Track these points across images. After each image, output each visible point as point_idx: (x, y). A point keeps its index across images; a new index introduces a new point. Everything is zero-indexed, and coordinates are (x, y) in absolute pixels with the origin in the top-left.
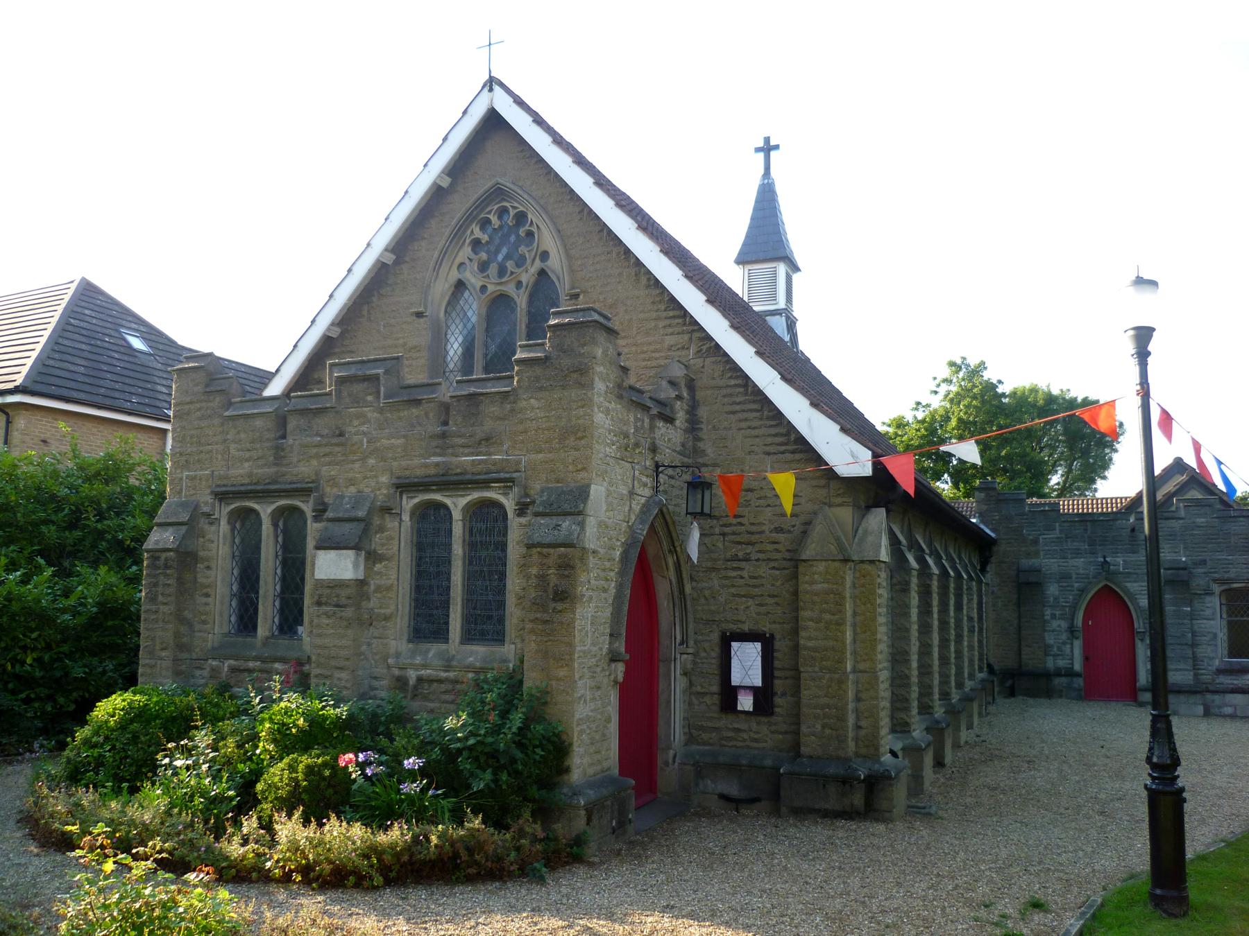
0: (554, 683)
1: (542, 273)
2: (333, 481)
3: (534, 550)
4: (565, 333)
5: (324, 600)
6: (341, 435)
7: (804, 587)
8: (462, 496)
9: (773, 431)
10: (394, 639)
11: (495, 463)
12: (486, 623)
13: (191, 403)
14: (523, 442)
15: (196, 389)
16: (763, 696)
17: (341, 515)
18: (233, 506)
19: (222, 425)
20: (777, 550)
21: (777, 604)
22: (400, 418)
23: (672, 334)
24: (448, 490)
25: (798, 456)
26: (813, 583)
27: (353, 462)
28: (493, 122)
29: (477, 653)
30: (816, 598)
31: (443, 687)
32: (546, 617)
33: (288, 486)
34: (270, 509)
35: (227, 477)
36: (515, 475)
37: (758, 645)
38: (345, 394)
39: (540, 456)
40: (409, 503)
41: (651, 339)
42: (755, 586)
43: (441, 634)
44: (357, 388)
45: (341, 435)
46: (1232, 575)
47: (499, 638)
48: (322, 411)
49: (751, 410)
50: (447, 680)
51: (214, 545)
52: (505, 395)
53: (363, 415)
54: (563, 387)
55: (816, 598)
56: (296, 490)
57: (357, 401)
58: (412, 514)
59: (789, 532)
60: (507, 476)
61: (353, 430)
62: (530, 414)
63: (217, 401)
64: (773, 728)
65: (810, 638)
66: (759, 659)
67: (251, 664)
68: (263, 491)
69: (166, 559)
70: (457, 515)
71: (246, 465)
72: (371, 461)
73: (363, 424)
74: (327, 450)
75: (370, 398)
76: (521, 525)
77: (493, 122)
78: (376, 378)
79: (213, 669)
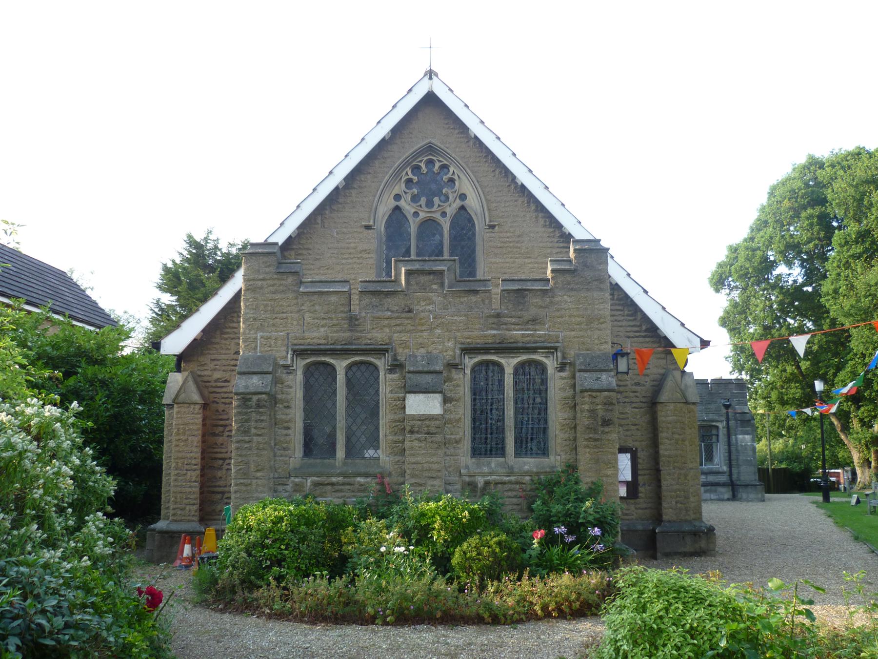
0: (604, 479)
1: (463, 208)
2: (405, 345)
3: (586, 394)
4: (587, 255)
5: (416, 429)
6: (410, 311)
8: (513, 357)
9: (631, 323)
10: (464, 458)
11: (540, 336)
12: (534, 439)
13: (263, 280)
14: (560, 323)
15: (267, 270)
16: (632, 487)
17: (421, 369)
18: (308, 361)
19: (297, 298)
20: (637, 397)
21: (638, 429)
22: (462, 303)
24: (501, 353)
25: (647, 339)
26: (667, 416)
27: (422, 331)
28: (431, 101)
29: (530, 463)
30: (669, 425)
31: (507, 487)
32: (597, 436)
33: (364, 347)
35: (304, 338)
36: (557, 345)
37: (629, 455)
38: (413, 282)
39: (573, 333)
40: (470, 362)
43: (499, 450)
44: (423, 279)
45: (410, 311)
47: (544, 451)
48: (389, 294)
49: (617, 310)
50: (510, 482)
52: (544, 292)
54: (588, 290)
55: (669, 425)
57: (424, 288)
59: (644, 385)
61: (421, 309)
63: (290, 279)
65: (666, 450)
66: (629, 463)
67: (334, 479)
68: (331, 350)
69: (258, 400)
70: (509, 371)
71: (322, 330)
72: (438, 331)
73: (429, 304)
74: (398, 322)
75: (434, 287)
77: (431, 101)
78: (441, 273)
79: (296, 485)
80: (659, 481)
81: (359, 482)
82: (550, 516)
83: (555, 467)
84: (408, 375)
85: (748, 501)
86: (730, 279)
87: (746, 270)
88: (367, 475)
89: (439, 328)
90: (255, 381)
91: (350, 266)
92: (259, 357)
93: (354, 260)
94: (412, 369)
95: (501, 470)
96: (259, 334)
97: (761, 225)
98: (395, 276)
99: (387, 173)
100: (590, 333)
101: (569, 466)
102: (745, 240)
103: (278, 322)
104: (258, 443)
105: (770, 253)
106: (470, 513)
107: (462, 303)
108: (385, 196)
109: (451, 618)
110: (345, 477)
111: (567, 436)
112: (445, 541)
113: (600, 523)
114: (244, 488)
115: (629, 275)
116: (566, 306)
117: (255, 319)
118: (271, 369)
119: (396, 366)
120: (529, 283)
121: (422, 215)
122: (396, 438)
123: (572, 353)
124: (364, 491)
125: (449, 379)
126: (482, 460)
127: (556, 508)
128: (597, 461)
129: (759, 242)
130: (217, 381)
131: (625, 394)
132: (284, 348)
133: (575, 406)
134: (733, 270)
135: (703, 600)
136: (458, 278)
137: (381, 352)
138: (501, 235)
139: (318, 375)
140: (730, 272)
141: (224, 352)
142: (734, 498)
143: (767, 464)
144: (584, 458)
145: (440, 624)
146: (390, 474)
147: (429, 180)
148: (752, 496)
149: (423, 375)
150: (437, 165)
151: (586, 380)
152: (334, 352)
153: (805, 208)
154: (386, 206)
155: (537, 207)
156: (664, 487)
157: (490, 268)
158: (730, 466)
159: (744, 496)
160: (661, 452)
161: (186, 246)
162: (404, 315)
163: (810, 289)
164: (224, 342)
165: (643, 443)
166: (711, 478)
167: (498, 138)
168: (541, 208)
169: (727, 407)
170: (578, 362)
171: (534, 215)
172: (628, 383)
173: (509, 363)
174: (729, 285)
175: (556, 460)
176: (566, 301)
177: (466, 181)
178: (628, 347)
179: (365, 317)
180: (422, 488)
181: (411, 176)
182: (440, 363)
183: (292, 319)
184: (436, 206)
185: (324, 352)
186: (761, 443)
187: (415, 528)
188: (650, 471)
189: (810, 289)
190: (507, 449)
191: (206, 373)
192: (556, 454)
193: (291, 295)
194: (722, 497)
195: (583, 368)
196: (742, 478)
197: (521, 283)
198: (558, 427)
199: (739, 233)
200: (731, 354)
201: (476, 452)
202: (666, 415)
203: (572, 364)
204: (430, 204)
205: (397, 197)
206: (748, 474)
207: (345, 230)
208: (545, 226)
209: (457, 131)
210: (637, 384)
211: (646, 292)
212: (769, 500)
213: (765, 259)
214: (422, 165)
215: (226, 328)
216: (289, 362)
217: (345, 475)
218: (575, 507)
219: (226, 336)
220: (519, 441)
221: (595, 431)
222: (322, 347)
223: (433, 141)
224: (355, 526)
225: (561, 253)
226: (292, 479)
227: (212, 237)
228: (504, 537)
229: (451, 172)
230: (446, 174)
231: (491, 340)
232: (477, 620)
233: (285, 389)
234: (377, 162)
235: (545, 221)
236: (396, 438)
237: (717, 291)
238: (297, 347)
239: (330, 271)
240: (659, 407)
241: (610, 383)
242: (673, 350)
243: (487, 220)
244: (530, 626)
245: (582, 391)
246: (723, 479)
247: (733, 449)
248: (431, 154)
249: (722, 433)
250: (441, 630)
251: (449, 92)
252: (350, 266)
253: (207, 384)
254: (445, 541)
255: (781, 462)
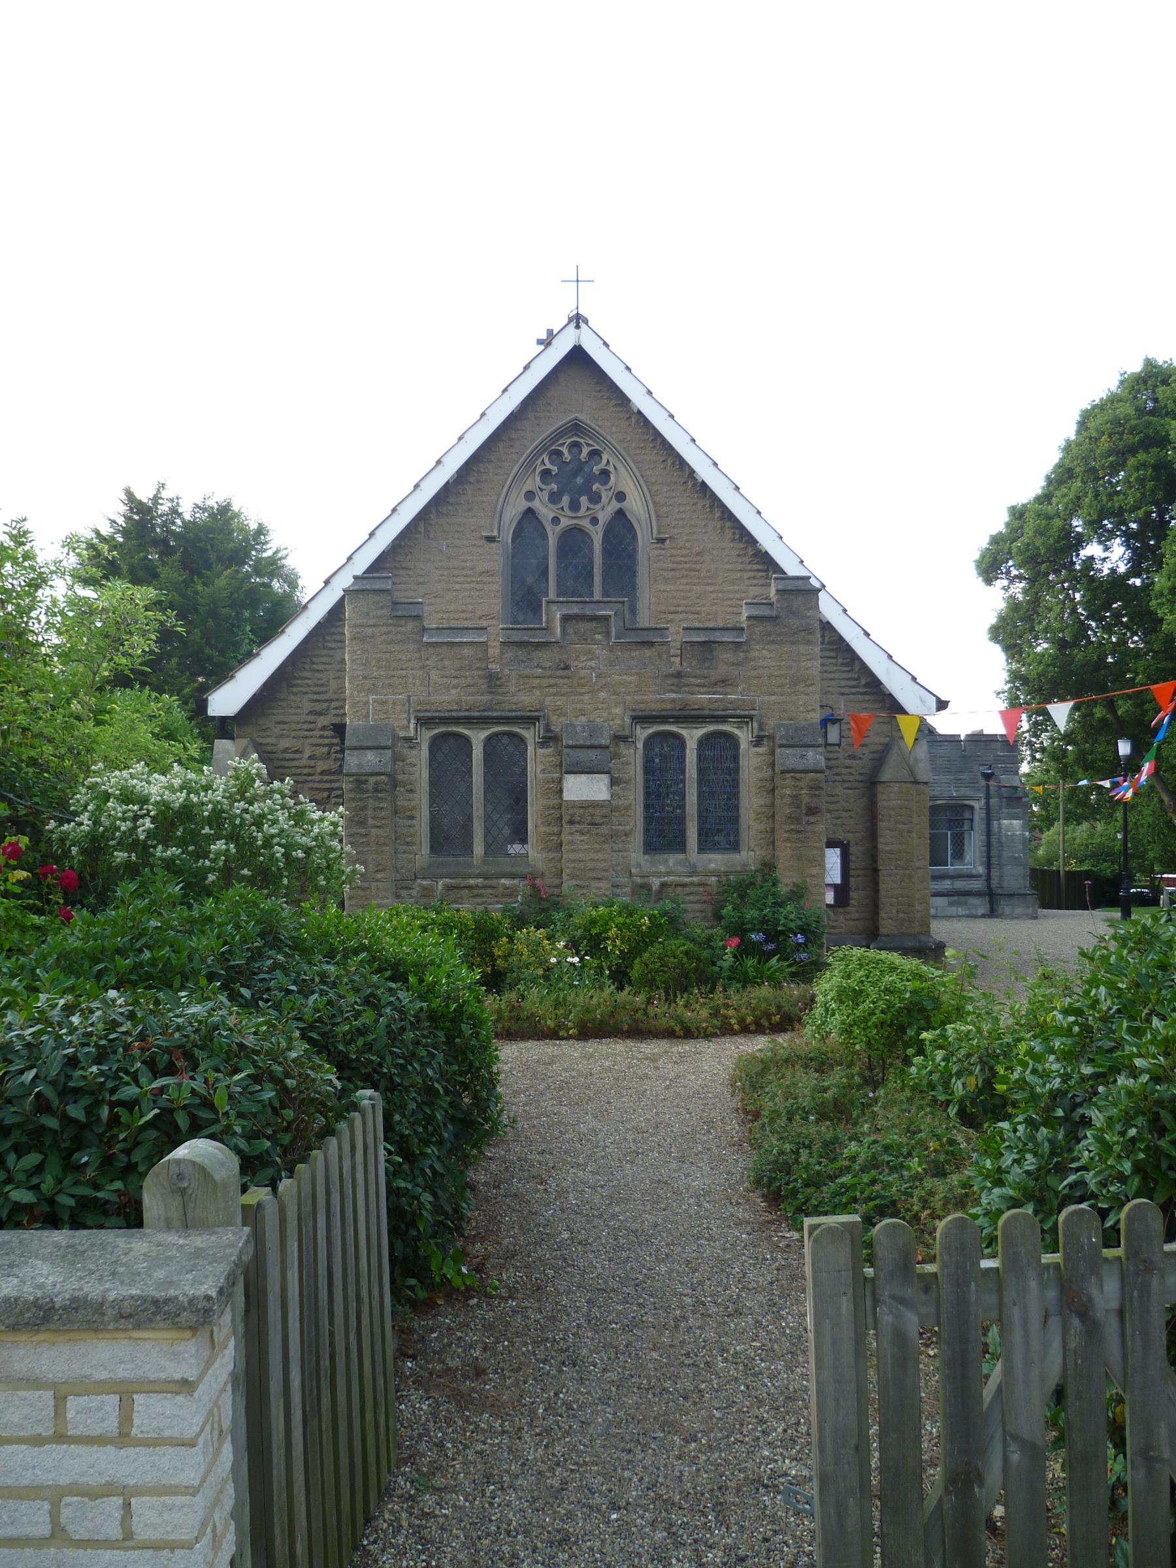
1: (620, 513)
3: (788, 775)
6: (567, 668)
7: (881, 803)
9: (846, 675)
10: (636, 855)
12: (721, 830)
15: (380, 612)
16: (842, 892)
17: (582, 742)
18: (436, 731)
19: (419, 651)
20: (851, 774)
21: (851, 817)
22: (633, 658)
23: (756, 585)
24: (682, 722)
25: (867, 697)
27: (582, 694)
29: (716, 861)
32: (799, 828)
34: (484, 734)
35: (429, 703)
36: (753, 712)
37: (838, 850)
38: (570, 631)
39: (773, 698)
40: (642, 733)
41: (737, 588)
42: (832, 803)
43: (679, 845)
44: (583, 626)
45: (567, 668)
46: (937, 793)
48: (539, 646)
50: (692, 884)
51: (417, 769)
52: (738, 645)
53: (590, 652)
54: (793, 643)
56: (517, 718)
57: (584, 639)
58: (646, 744)
60: (747, 713)
61: (581, 665)
62: (762, 663)
63: (410, 626)
64: (848, 917)
67: (472, 882)
69: (376, 783)
70: (691, 746)
71: (453, 691)
72: (603, 694)
73: (591, 660)
74: (552, 681)
75: (598, 637)
76: (758, 754)
78: (606, 618)
79: (424, 888)
80: (876, 884)
81: (503, 885)
82: (743, 924)
83: (749, 865)
84: (565, 750)
85: (1013, 918)
86: (1010, 563)
87: (1033, 548)
88: (512, 876)
89: (603, 691)
90: (370, 758)
91: (467, 593)
92: (372, 727)
93: (473, 585)
94: (570, 742)
95: (681, 869)
96: (372, 698)
97: (1061, 476)
98: (548, 621)
99: (516, 462)
100: (793, 698)
101: (765, 864)
102: (1038, 500)
103: (396, 681)
104: (377, 836)
105: (1075, 523)
106: (650, 919)
107: (633, 658)
108: (513, 495)
109: (638, 1032)
110: (485, 878)
111: (762, 827)
112: (622, 952)
113: (803, 931)
114: (361, 893)
115: (845, 611)
116: (764, 663)
117: (365, 678)
118: (389, 743)
119: (549, 739)
120: (718, 633)
121: (565, 522)
122: (549, 829)
123: (771, 723)
124: (510, 896)
125: (616, 756)
126: (657, 857)
127: (752, 914)
128: (799, 858)
129: (1058, 505)
130: (285, 751)
131: (835, 770)
132: (405, 716)
133: (773, 790)
134: (1014, 551)
135: (896, 968)
136: (628, 626)
137: (529, 721)
138: (674, 552)
139: (449, 750)
140: (1010, 552)
141: (293, 711)
142: (992, 913)
143: (1059, 865)
144: (784, 854)
145: (628, 1037)
146: (543, 875)
147: (576, 476)
148: (1019, 910)
149: (585, 750)
150: (585, 450)
151: (788, 758)
152: (468, 721)
153: (1133, 451)
154: (515, 508)
155: (723, 513)
156: (882, 892)
157: (659, 598)
158: (989, 866)
159: (1007, 910)
160: (880, 846)
161: (123, 509)
162: (559, 673)
163: (1138, 582)
164: (292, 697)
165: (858, 835)
166: (960, 885)
167: (672, 416)
168: (727, 516)
169: (988, 777)
170: (778, 736)
171: (719, 525)
172: (840, 755)
173: (692, 736)
174: (1008, 572)
175: (748, 857)
176: (765, 656)
177: (626, 474)
178: (842, 708)
179: (509, 676)
180: (584, 891)
181: (548, 466)
182: (606, 734)
183: (414, 677)
184: (583, 509)
185: (457, 721)
186: (1052, 830)
187: (582, 938)
188: (865, 868)
189: (1138, 582)
190: (688, 843)
191: (269, 740)
192: (750, 850)
193: (411, 647)
194: (974, 912)
195: (785, 742)
196: (1005, 884)
197: (707, 632)
198: (753, 815)
199: (1028, 486)
200: (1007, 687)
201: (650, 847)
202: (889, 800)
203: (771, 738)
204: (575, 506)
205: (530, 495)
206: (1014, 878)
207: (457, 542)
208: (733, 540)
209: (613, 402)
210: (852, 757)
211: (867, 634)
212: (1045, 916)
213: (1067, 531)
214: (564, 450)
215: (295, 678)
216: (412, 733)
217: (486, 877)
218: (774, 912)
219: (295, 690)
220: (702, 833)
221: (798, 821)
222: (454, 714)
223: (580, 416)
224: (508, 936)
225: (754, 578)
226: (419, 881)
227: (165, 494)
228: (690, 946)
229: (604, 461)
230: (597, 464)
231: (669, 706)
232: (669, 1034)
233: (407, 768)
234: (501, 445)
235: (734, 534)
236: (549, 829)
237: (989, 581)
238: (422, 714)
239: (438, 600)
240: (880, 788)
241: (818, 762)
242: (900, 717)
243: (655, 531)
244: (727, 1039)
245: (783, 772)
246: (978, 885)
247: (994, 840)
248: (576, 435)
249: (979, 816)
250: (630, 1043)
251: (604, 348)
252: (467, 593)
253: (272, 756)
254: (622, 952)
255: (1082, 861)
